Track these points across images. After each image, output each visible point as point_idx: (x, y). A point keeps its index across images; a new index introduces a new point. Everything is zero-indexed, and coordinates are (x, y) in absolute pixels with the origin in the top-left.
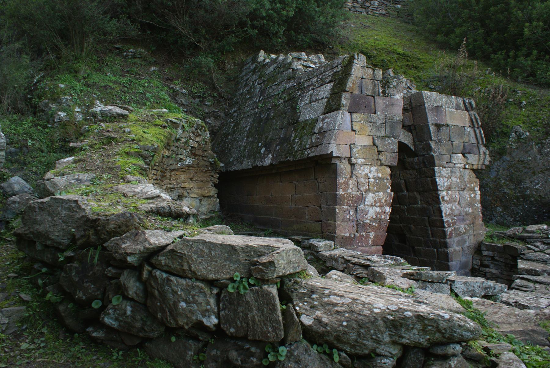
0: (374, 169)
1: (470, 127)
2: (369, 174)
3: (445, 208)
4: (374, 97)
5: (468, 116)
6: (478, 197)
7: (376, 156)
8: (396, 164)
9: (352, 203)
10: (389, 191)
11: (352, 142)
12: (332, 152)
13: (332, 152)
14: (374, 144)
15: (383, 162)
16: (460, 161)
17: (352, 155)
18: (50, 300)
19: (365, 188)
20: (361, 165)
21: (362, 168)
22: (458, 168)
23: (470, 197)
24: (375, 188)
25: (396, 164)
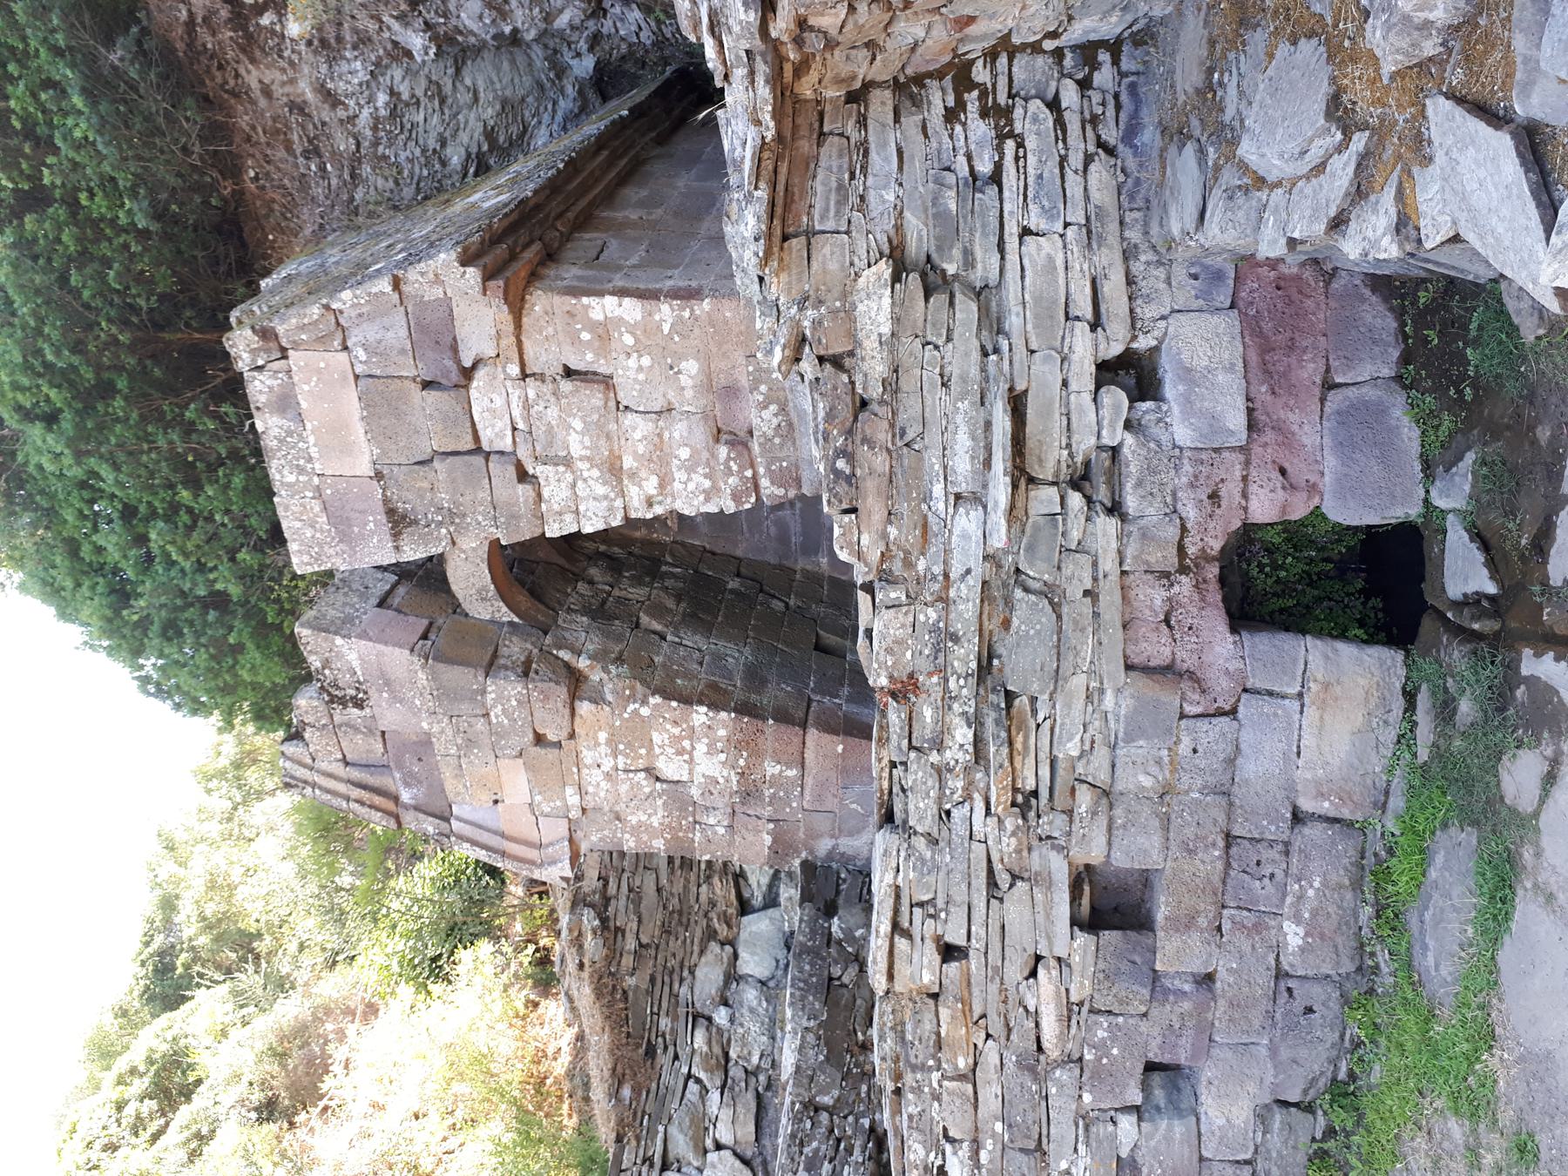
6: (630, 309)
16: (499, 402)
22: (527, 418)
24: (643, 751)
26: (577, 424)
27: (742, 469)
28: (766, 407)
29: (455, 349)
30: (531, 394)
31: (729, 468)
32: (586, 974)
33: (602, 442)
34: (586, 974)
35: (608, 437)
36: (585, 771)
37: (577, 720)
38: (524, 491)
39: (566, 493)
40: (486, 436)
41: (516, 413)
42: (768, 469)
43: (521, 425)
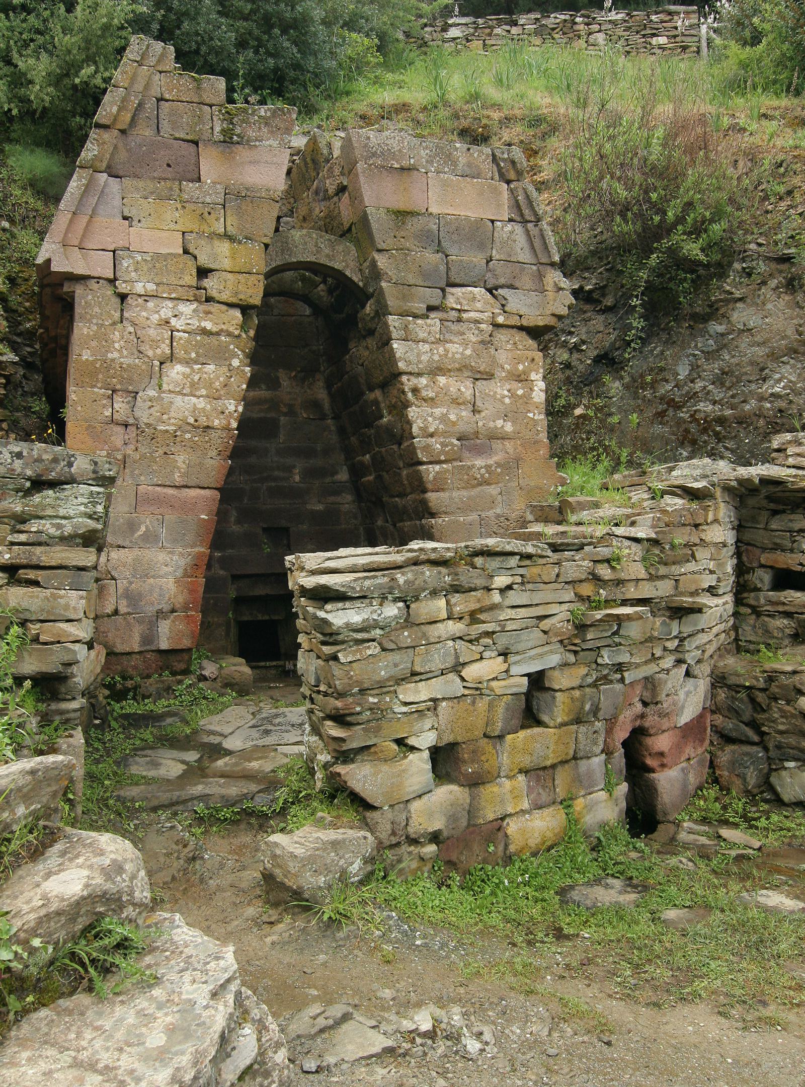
0: (187, 309)
1: (511, 220)
2: (173, 321)
3: (420, 417)
4: (196, 143)
5: (506, 195)
6: (539, 395)
7: (193, 281)
8: (257, 300)
9: (121, 383)
10: (236, 363)
11: (121, 244)
12: (48, 261)
13: (48, 261)
14: (186, 252)
15: (214, 293)
16: (479, 305)
17: (118, 274)
18: (401, 374)
19: (159, 351)
20: (147, 297)
21: (150, 304)
22: (469, 321)
23: (513, 395)
24: (193, 355)
25: (257, 300)
26: (468, 352)
27: (447, 453)
28: (487, 472)
29: (511, 287)
30: (483, 326)
31: (447, 446)
32: (61, 668)
33: (457, 366)
34: (61, 668)
35: (459, 370)
36: (170, 304)
37: (224, 308)
38: (421, 307)
39: (422, 335)
40: (458, 291)
41: (472, 315)
42: (447, 471)
43: (465, 315)
